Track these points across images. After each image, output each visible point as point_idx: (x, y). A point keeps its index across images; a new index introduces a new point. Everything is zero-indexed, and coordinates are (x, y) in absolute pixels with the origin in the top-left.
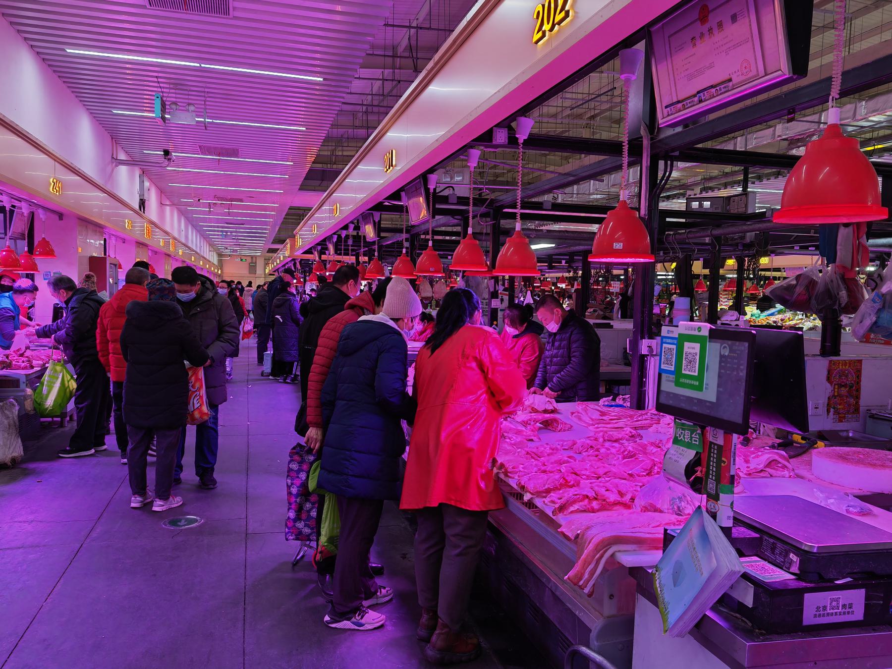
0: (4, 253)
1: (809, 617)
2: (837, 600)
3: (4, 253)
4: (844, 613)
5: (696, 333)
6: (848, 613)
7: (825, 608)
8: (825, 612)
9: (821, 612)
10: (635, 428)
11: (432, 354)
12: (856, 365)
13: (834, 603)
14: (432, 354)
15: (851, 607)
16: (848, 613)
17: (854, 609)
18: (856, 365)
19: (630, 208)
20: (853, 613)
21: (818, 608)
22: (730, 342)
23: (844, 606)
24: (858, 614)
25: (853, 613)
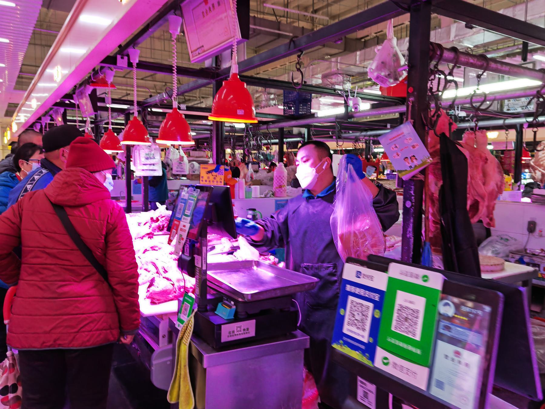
0: (415, 93)
1: (225, 338)
2: (240, 327)
3: (415, 93)
4: (244, 333)
5: (420, 282)
6: (247, 333)
7: (233, 332)
8: (234, 334)
9: (232, 334)
10: (16, 202)
11: (51, 202)
12: (385, 269)
13: (239, 329)
14: (51, 202)
15: (248, 329)
16: (247, 333)
17: (250, 330)
18: (385, 269)
19: (371, 180)
20: (249, 333)
21: (230, 333)
22: (456, 300)
23: (244, 330)
24: (252, 333)
25: (249, 333)
